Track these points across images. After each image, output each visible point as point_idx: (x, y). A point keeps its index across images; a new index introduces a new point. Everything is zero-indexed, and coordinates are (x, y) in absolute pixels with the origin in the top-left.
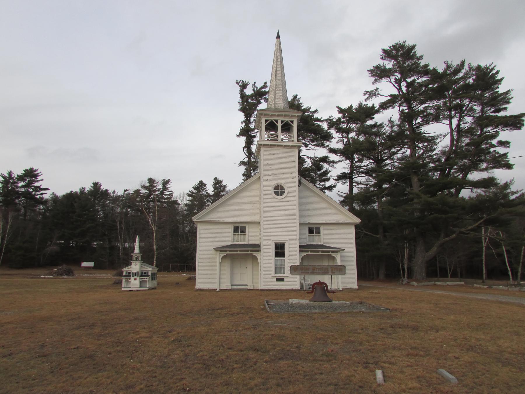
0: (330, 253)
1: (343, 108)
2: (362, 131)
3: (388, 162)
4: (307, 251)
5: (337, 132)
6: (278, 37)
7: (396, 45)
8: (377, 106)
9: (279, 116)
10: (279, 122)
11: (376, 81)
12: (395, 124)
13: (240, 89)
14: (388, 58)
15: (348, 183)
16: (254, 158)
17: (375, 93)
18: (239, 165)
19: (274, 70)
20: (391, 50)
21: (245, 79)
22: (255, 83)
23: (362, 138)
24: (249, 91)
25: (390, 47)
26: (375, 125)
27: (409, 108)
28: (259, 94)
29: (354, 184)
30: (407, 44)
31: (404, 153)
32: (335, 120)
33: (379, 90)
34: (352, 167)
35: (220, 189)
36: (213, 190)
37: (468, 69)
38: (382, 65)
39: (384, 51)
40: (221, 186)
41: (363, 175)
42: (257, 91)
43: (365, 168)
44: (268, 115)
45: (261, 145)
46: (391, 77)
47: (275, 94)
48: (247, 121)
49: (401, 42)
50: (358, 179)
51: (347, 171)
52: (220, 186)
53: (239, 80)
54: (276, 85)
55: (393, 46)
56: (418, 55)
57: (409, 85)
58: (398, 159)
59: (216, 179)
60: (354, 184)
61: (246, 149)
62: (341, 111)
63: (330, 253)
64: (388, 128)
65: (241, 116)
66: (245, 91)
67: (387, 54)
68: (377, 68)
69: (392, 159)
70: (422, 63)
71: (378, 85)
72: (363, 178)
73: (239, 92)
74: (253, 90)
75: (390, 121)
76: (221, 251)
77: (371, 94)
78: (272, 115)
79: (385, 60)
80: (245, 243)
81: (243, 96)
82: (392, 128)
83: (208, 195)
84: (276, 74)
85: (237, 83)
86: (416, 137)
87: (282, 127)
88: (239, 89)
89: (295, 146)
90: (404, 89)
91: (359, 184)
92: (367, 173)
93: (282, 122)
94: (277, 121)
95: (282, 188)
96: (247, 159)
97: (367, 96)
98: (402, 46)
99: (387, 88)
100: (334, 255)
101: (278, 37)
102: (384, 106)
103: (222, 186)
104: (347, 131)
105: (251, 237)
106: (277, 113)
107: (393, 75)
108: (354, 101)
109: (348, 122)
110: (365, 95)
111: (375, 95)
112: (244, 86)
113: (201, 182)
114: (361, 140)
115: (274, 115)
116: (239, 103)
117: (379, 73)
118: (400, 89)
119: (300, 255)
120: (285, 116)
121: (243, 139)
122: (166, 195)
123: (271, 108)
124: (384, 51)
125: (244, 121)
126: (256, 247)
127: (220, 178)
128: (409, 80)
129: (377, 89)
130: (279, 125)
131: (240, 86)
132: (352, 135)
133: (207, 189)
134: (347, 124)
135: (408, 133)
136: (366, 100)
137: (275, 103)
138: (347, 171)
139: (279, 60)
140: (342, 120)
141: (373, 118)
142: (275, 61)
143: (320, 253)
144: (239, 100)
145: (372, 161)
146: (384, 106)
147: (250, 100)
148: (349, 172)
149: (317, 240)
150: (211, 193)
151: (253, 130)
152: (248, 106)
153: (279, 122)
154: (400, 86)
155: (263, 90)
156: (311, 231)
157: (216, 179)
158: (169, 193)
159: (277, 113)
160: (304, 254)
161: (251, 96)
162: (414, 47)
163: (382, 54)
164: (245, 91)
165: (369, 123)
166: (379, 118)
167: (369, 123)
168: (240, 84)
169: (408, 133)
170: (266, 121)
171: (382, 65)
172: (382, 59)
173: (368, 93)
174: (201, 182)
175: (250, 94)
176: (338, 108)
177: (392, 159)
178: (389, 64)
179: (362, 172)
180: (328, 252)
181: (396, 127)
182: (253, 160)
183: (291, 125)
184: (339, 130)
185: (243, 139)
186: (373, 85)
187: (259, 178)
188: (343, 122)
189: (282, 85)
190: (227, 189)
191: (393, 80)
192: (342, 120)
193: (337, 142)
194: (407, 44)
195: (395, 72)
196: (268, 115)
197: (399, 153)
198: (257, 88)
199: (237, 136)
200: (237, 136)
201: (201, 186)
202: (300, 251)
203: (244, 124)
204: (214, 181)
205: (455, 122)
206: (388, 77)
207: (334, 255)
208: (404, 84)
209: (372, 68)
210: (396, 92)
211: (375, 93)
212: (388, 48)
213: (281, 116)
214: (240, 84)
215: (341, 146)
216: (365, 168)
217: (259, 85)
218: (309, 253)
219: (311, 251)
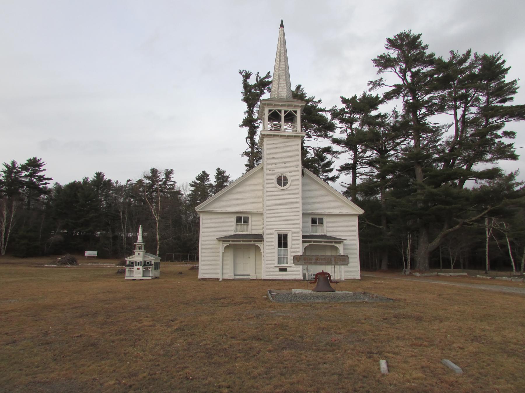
0: (333, 244)
1: (347, 98)
3: (392, 152)
4: (310, 242)
5: (340, 123)
6: (282, 25)
7: (401, 34)
8: (381, 96)
9: (282, 106)
10: (283, 112)
11: (380, 71)
12: (400, 114)
14: (393, 47)
15: (351, 174)
16: (257, 149)
17: (379, 83)
20: (396, 40)
21: (249, 69)
22: (258, 73)
23: (366, 128)
24: (252, 81)
25: (395, 37)
26: (379, 116)
27: (414, 98)
29: (357, 175)
31: (408, 143)
33: (384, 80)
35: (223, 179)
36: (215, 180)
37: (474, 58)
39: (389, 40)
40: (223, 177)
41: (367, 166)
43: (369, 158)
44: (271, 105)
45: (264, 135)
47: (278, 84)
48: (250, 112)
49: (407, 31)
50: (362, 170)
51: (351, 162)
52: (222, 176)
53: (242, 69)
54: (279, 75)
55: (398, 35)
56: (423, 45)
57: (413, 75)
58: (402, 150)
59: (218, 169)
61: (249, 140)
62: (345, 101)
63: (333, 244)
64: (392, 119)
65: (244, 107)
66: (248, 80)
67: (392, 43)
68: (382, 57)
69: (396, 150)
70: (428, 52)
71: (382, 75)
72: (366, 169)
74: (257, 80)
75: (395, 112)
76: (224, 241)
77: (375, 84)
78: (275, 105)
80: (248, 233)
81: (246, 86)
82: (396, 119)
85: (241, 73)
86: (421, 128)
87: (285, 117)
88: (241, 79)
89: (298, 136)
90: (409, 79)
91: (362, 174)
92: (371, 163)
93: (285, 112)
94: (280, 111)
95: (285, 178)
96: (250, 150)
97: (371, 86)
98: (407, 36)
99: (392, 78)
100: (336, 245)
101: (282, 25)
102: (388, 96)
104: (351, 121)
105: (254, 227)
106: (280, 103)
107: (398, 65)
108: (358, 90)
109: (352, 112)
110: (369, 84)
111: (379, 85)
112: (247, 76)
113: (204, 172)
114: (365, 130)
115: (278, 105)
116: (242, 93)
117: (384, 63)
118: (404, 79)
119: (303, 246)
120: (289, 106)
121: (246, 130)
122: (168, 185)
123: (274, 98)
124: (389, 40)
125: (247, 112)
126: (259, 238)
127: (222, 169)
128: (414, 70)
129: (381, 79)
130: (283, 115)
131: (243, 76)
132: (356, 125)
134: (351, 115)
135: (412, 124)
136: (370, 90)
137: (278, 93)
138: (351, 162)
139: (283, 50)
140: (346, 110)
141: (377, 109)
143: (323, 244)
144: (242, 90)
146: (388, 96)
147: (253, 91)
148: (352, 163)
149: (320, 231)
150: (214, 184)
151: (256, 120)
153: (283, 112)
154: (405, 76)
155: (267, 80)
156: (314, 222)
157: (218, 169)
158: (171, 183)
159: (280, 103)
160: (307, 244)
161: (255, 86)
162: (419, 36)
163: (387, 43)
164: (248, 80)
165: (373, 113)
166: (383, 109)
167: (373, 113)
168: (244, 74)
169: (412, 124)
170: (270, 111)
172: (387, 48)
173: (372, 83)
174: (204, 172)
176: (342, 98)
177: (396, 150)
178: (394, 54)
180: (331, 242)
181: (400, 117)
182: (256, 151)
183: (294, 115)
185: (246, 130)
186: (377, 75)
187: (262, 168)
188: (347, 113)
191: (398, 70)
192: (346, 110)
193: (341, 133)
195: (400, 61)
196: (271, 105)
198: (260, 78)
199: (240, 126)
200: (240, 126)
201: (203, 176)
202: (303, 242)
203: (247, 114)
204: (217, 172)
205: (460, 112)
207: (336, 245)
208: (408, 74)
209: (376, 58)
210: (400, 82)
213: (284, 105)
214: (244, 74)
215: (344, 136)
216: (369, 158)
217: (262, 75)
218: (312, 243)
219: (314, 242)
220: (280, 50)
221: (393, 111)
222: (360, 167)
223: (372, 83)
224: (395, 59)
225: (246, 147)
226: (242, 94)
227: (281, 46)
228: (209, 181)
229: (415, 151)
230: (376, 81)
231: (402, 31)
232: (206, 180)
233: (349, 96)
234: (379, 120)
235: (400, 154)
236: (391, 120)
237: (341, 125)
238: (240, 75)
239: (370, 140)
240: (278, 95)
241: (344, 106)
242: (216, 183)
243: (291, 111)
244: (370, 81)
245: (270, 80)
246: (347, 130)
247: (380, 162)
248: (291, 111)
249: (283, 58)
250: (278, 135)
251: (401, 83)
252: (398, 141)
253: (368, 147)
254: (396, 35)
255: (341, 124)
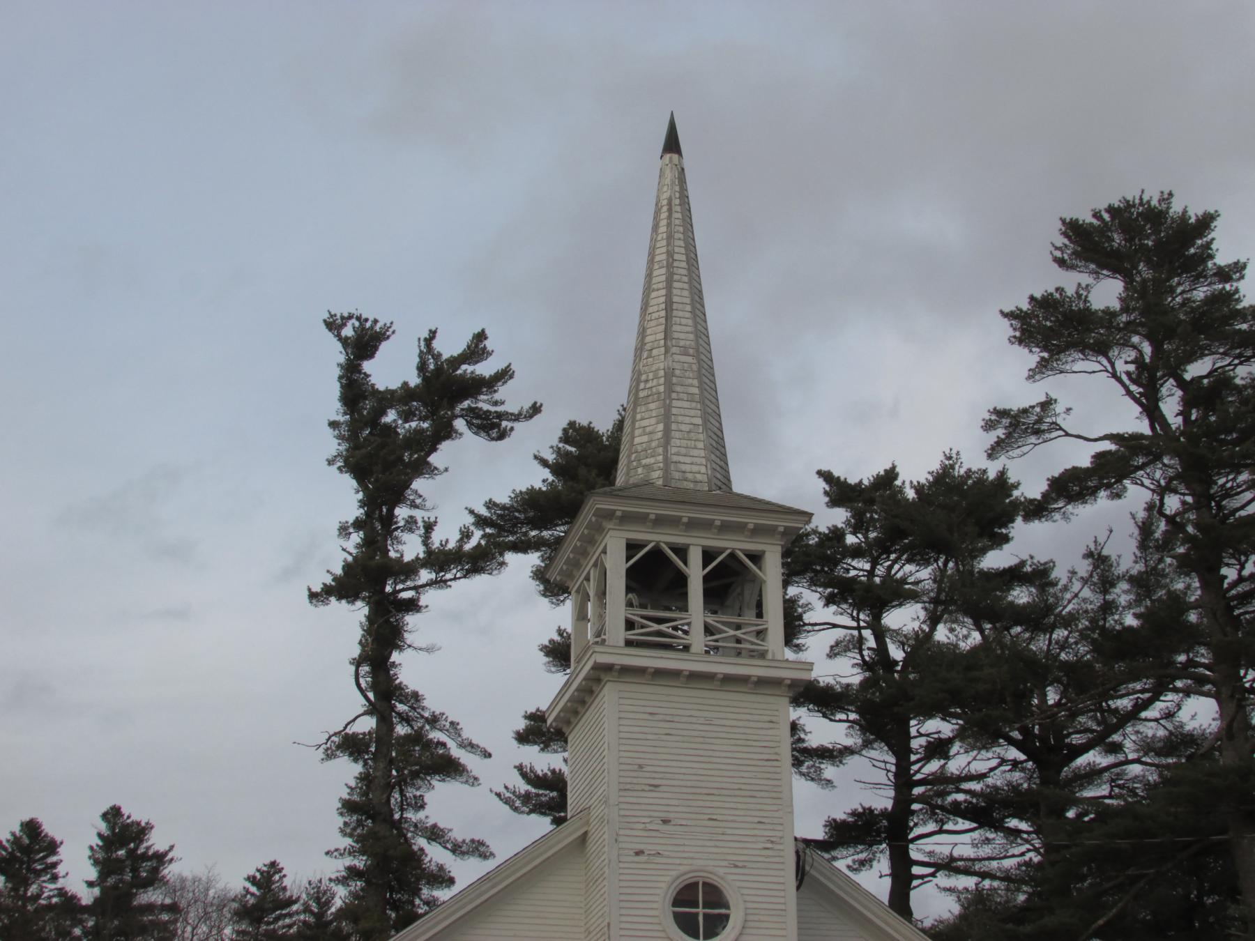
1: (853, 480)
2: (972, 596)
3: (1094, 757)
5: (829, 600)
6: (672, 144)
7: (1129, 205)
8: (1032, 488)
9: (693, 525)
10: (695, 557)
12: (1121, 569)
13: (342, 359)
14: (1087, 260)
15: (883, 864)
16: (406, 719)
17: (1040, 421)
18: (329, 755)
19: (658, 298)
20: (1104, 229)
21: (375, 311)
22: (433, 334)
23: (960, 635)
24: (392, 369)
25: (1097, 215)
26: (1014, 575)
27: (1203, 499)
28: (453, 392)
29: (916, 870)
30: (1176, 208)
31: (1169, 715)
32: (813, 540)
33: (1059, 408)
34: (903, 781)
35: (135, 870)
36: (92, 874)
38: (1070, 291)
39: (1073, 229)
40: (136, 859)
41: (968, 825)
42: (439, 369)
43: (976, 786)
44: (640, 519)
45: (608, 668)
46: (1114, 352)
47: (667, 418)
48: (376, 524)
49: (1153, 196)
50: (942, 846)
51: (883, 801)
52: (132, 853)
53: (341, 310)
54: (669, 374)
55: (1110, 209)
56: (1222, 258)
57: (1194, 395)
58: (1148, 747)
59: (113, 814)
60: (916, 870)
61: (365, 669)
62: (840, 492)
64: (1086, 593)
65: (346, 500)
66: (367, 366)
67: (1087, 243)
68: (1045, 304)
69: (1116, 748)
71: (1049, 386)
72: (962, 841)
73: (338, 372)
74: (422, 367)
75: (1099, 560)
77: (1017, 427)
78: (660, 521)
79: (1072, 267)
81: (354, 389)
82: (1105, 592)
83: (69, 903)
84: (668, 318)
85: (334, 325)
87: (706, 579)
88: (335, 354)
92: (987, 812)
93: (708, 556)
94: (682, 552)
95: (715, 897)
96: (368, 724)
97: (1000, 432)
98: (1154, 216)
101: (672, 144)
103: (145, 857)
104: (872, 600)
106: (686, 514)
107: (1126, 344)
109: (875, 552)
110: (989, 426)
111: (1037, 432)
112: (365, 343)
113: (32, 827)
114: (965, 646)
115: (673, 522)
116: (333, 425)
118: (1151, 410)
120: (726, 528)
121: (350, 619)
123: (648, 483)
124: (1073, 229)
125: (358, 524)
127: (135, 812)
128: (1197, 369)
129: (1047, 404)
130: (695, 573)
131: (345, 342)
132: (904, 618)
133: (61, 870)
134: (874, 564)
136: (992, 453)
137: (666, 460)
138: (883, 801)
139: (680, 256)
140: (851, 539)
141: (1006, 539)
142: (661, 257)
144: (334, 409)
145: (1014, 754)
146: (1070, 487)
147: (391, 417)
148: (889, 804)
150: (87, 896)
151: (409, 570)
152: (384, 446)
153: (695, 557)
155: (466, 368)
157: (113, 814)
159: (686, 514)
161: (403, 397)
162: (1206, 222)
163: (1061, 241)
164: (367, 366)
165: (994, 560)
166: (1026, 542)
167: (994, 560)
168: (348, 332)
170: (632, 547)
171: (1070, 291)
172: (1061, 262)
173: (1006, 421)
174: (32, 827)
175: (381, 388)
176: (827, 476)
177: (1116, 748)
179: (957, 810)
181: (1124, 586)
182: (401, 730)
184: (843, 592)
185: (350, 619)
186: (1029, 385)
187: (584, 838)
188: (857, 552)
189: (699, 376)
190: (170, 871)
192: (851, 539)
193: (836, 651)
194: (1176, 208)
195: (1130, 327)
196: (640, 519)
197: (1143, 715)
198: (437, 356)
199: (313, 596)
200: (313, 596)
201: (28, 851)
203: (357, 537)
204: (103, 827)
206: (1102, 349)
209: (1025, 306)
210: (1133, 421)
211: (1040, 421)
212: (1087, 217)
213: (706, 525)
214: (348, 332)
215: (845, 672)
216: (976, 786)
217: (450, 346)
220: (670, 254)
221: (1089, 555)
222: (931, 827)
223: (1006, 421)
224: (1109, 314)
225: (348, 707)
226: (330, 433)
227: (670, 237)
228: (55, 878)
229: (1226, 759)
230: (1025, 411)
231: (1132, 194)
232: (38, 874)
233: (860, 472)
234: (1021, 596)
235: (1135, 769)
236: (1079, 597)
237: (827, 614)
238: (330, 337)
239: (988, 695)
240: (666, 470)
241: (839, 516)
242: (96, 891)
243: (732, 555)
244: (996, 412)
245: (485, 369)
246: (861, 640)
247: (1042, 802)
248: (732, 555)
249: (682, 295)
250: (675, 674)
251: (1143, 427)
252: (1124, 703)
253: (981, 733)
254: (1102, 205)
255: (833, 608)
